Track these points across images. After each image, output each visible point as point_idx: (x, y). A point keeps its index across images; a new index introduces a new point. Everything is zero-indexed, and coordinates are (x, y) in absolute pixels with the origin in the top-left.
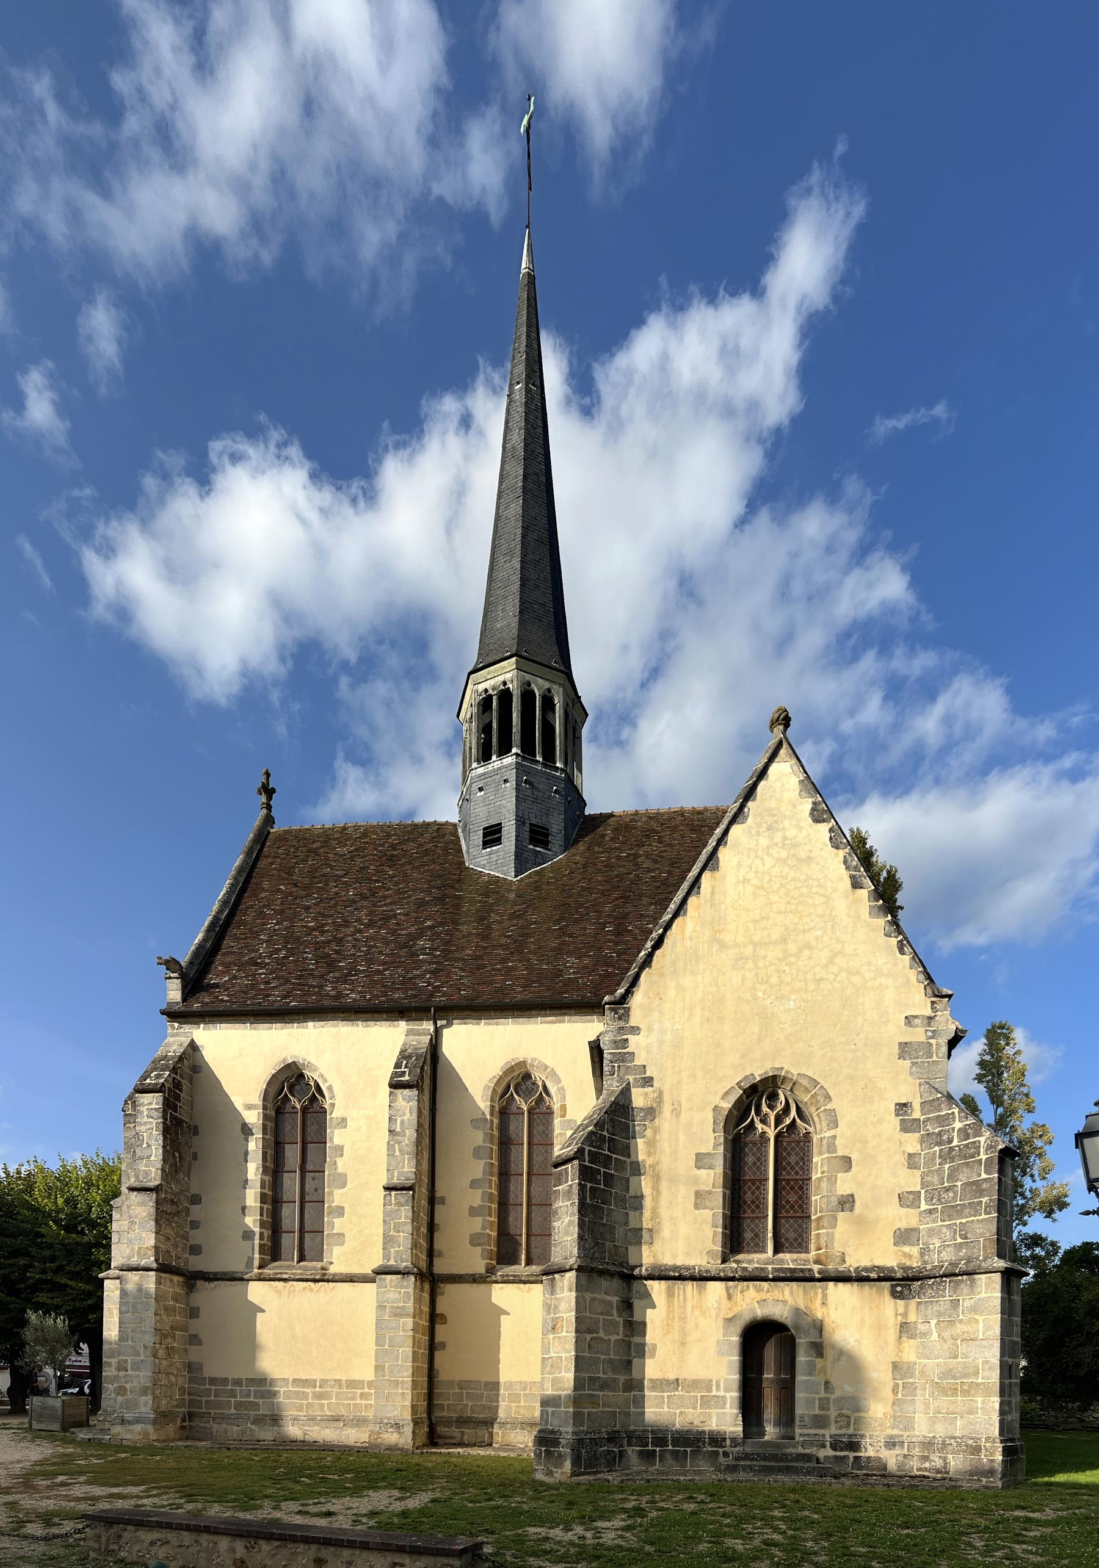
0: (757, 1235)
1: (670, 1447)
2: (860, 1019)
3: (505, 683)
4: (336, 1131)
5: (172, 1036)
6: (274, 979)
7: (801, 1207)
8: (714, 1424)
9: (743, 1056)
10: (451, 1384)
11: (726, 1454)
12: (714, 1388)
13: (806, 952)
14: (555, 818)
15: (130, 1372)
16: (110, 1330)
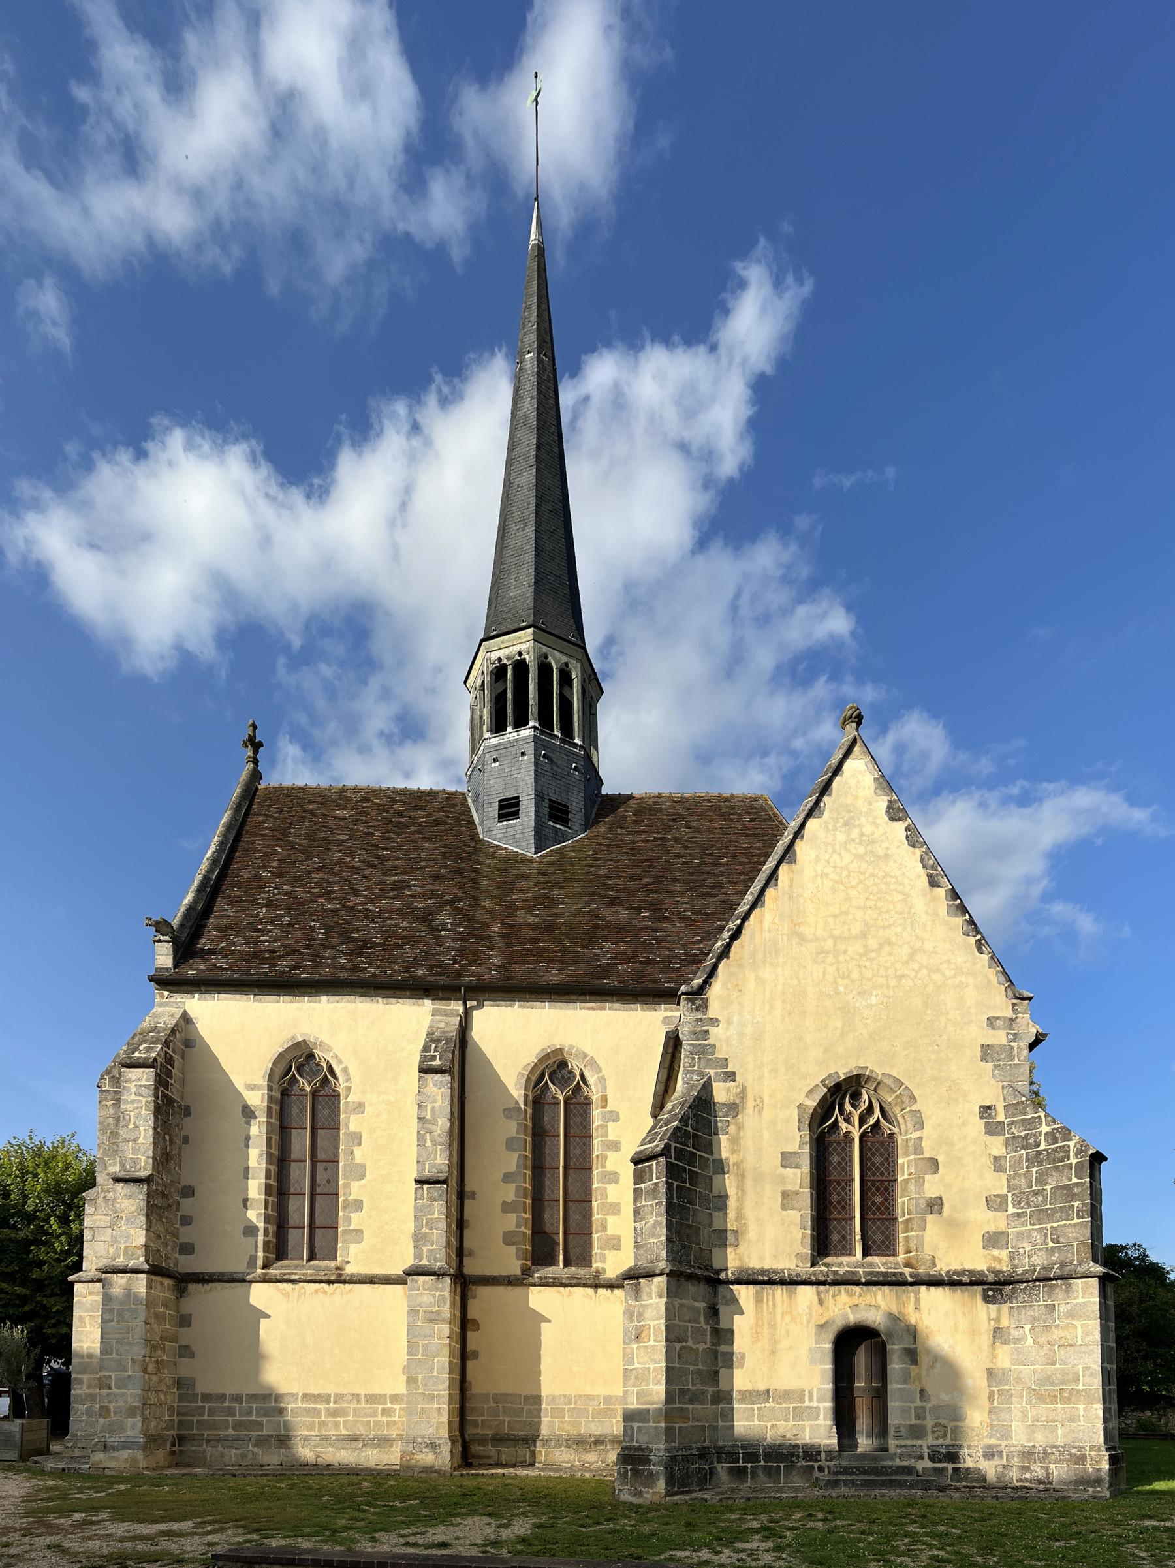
0: (844, 1237)
1: (762, 1463)
2: (943, 1019)
3: (520, 654)
4: (352, 1117)
5: (161, 1005)
6: (279, 947)
7: (887, 1208)
8: (807, 1437)
9: (826, 1051)
10: (485, 1397)
11: (821, 1469)
12: (807, 1398)
13: (887, 948)
14: (572, 794)
15: (114, 1390)
16: (80, 1341)
